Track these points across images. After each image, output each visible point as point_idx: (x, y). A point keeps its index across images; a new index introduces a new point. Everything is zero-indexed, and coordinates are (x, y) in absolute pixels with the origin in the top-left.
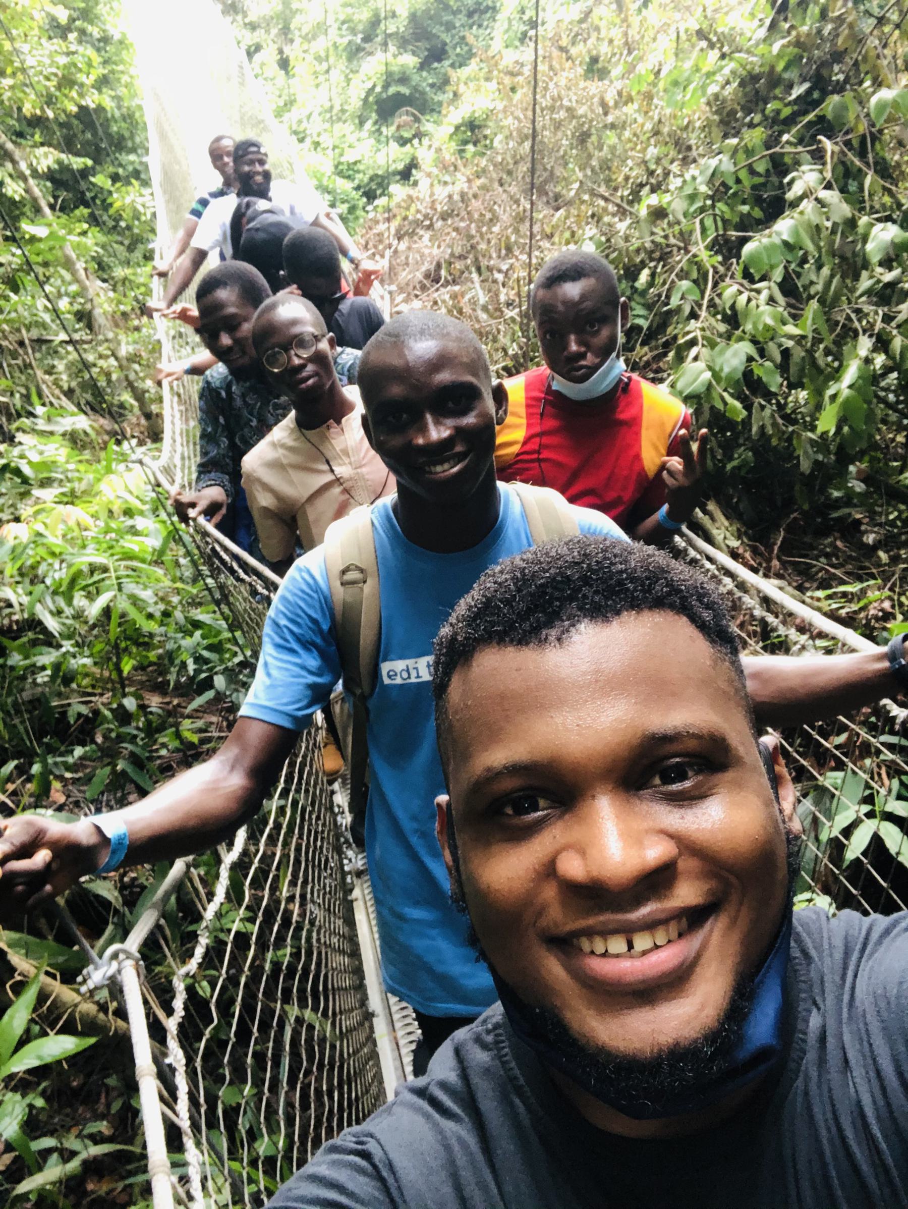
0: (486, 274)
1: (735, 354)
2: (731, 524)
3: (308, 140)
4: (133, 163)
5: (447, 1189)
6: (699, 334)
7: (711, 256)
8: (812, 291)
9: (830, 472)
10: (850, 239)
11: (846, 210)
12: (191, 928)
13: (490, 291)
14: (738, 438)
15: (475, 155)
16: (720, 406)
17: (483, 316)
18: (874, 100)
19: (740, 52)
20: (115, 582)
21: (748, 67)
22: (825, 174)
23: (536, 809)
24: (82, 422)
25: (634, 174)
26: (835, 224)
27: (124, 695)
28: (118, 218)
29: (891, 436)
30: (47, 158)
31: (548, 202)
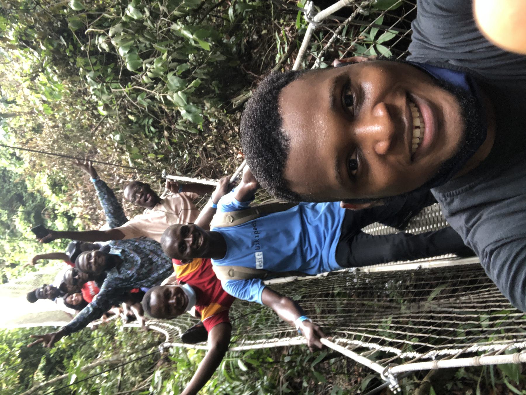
0: (119, 186)
1: (172, 80)
2: (243, 94)
5: (508, 219)
7: (128, 87)
8: (149, 46)
10: (131, 25)
11: (118, 25)
15: (67, 186)
16: (193, 89)
18: (74, 8)
19: (42, 64)
21: (49, 61)
22: (102, 33)
23: (356, 160)
24: (158, 374)
25: (87, 116)
26: (123, 31)
27: (283, 362)
30: (39, 376)
31: (92, 156)
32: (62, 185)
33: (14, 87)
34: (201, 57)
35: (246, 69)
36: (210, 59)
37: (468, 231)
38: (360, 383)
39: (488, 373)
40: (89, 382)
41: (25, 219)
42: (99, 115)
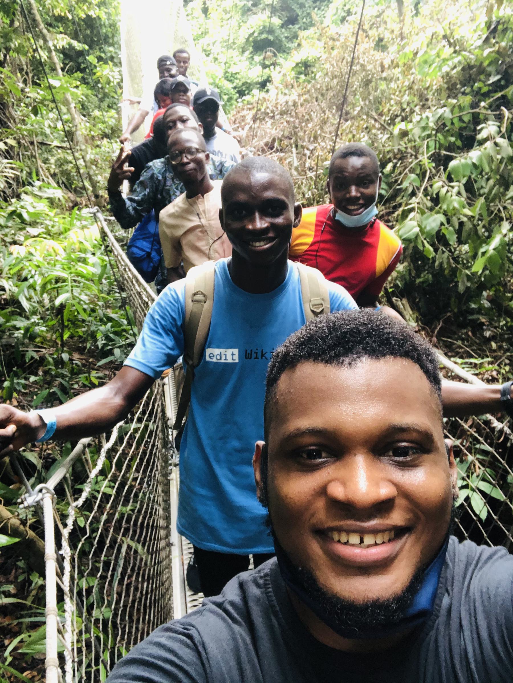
0: (300, 149)
1: (434, 220)
2: (413, 314)
3: (211, 56)
4: (111, 52)
5: (233, 663)
6: (416, 205)
8: (482, 192)
9: (473, 294)
12: (79, 487)
13: (300, 159)
14: (425, 266)
16: (421, 248)
17: (295, 173)
19: (465, 51)
20: (70, 288)
21: (468, 61)
22: (502, 129)
24: (58, 193)
25: (393, 108)
26: (502, 158)
27: (63, 352)
28: (99, 82)
29: (509, 279)
30: (63, 41)
32: (306, 75)
33: (437, 15)
34: (465, 262)
35: (445, 320)
36: (461, 271)
37: (220, 605)
38: (32, 451)
39: (36, 615)
40: (52, 105)
41: (264, 27)
42: (394, 124)
